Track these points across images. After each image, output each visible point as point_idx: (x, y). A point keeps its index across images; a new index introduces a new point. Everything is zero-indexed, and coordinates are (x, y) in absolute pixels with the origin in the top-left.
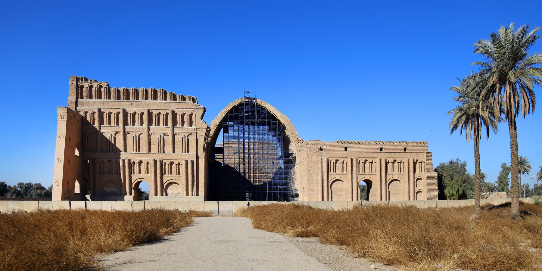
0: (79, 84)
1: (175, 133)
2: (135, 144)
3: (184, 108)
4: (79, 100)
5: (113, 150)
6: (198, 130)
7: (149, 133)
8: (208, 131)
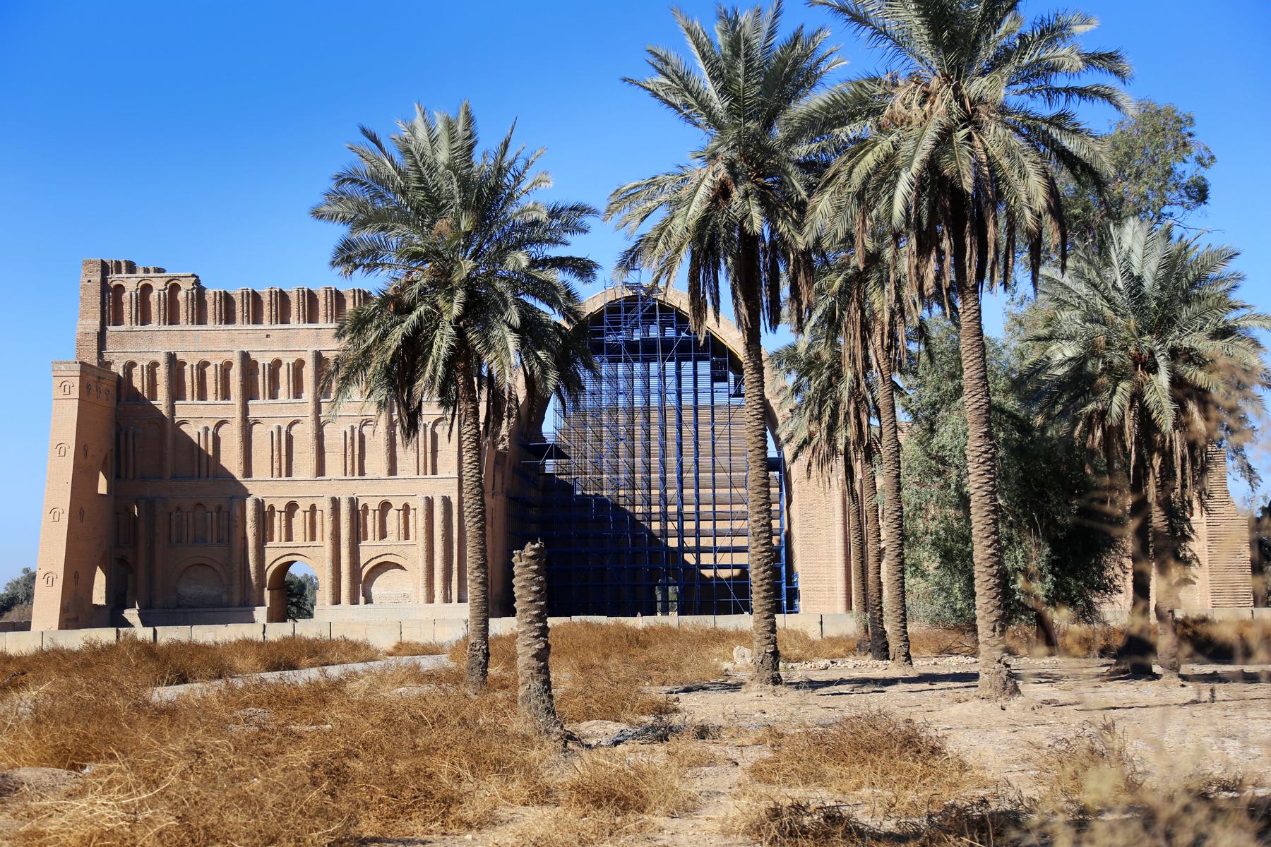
0: (109, 281)
2: (276, 453)
4: (110, 328)
5: (211, 474)
7: (317, 419)
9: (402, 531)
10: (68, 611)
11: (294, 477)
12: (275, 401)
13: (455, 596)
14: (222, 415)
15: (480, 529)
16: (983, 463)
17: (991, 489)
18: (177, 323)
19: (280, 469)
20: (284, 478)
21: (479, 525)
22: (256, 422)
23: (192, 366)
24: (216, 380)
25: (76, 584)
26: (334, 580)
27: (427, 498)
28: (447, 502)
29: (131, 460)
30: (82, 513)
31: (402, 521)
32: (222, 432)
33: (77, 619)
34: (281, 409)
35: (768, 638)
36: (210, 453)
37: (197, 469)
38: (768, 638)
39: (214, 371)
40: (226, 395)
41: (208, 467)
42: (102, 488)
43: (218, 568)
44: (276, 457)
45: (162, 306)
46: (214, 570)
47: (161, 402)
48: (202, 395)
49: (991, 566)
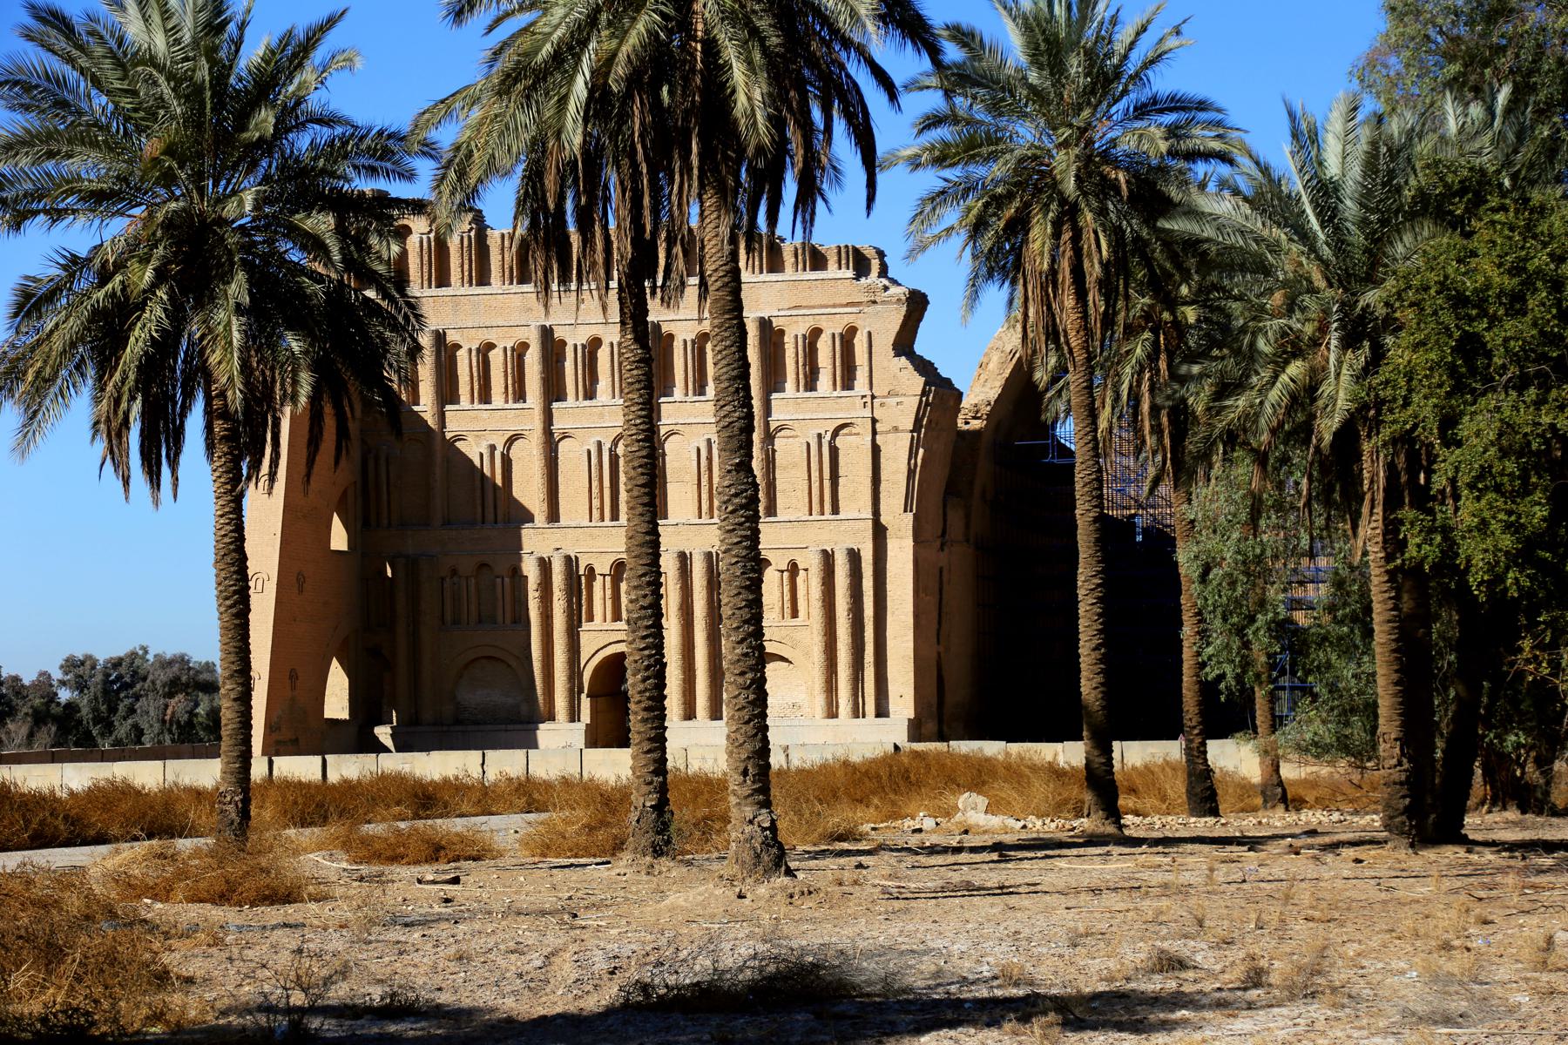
1: (773, 426)
2: (595, 484)
3: (813, 307)
5: (500, 517)
6: (882, 405)
8: (927, 404)
9: (787, 605)
10: (279, 729)
11: (563, 521)
12: (593, 402)
13: (870, 707)
14: (515, 427)
15: (236, 616)
16: (732, 512)
17: (744, 553)
18: (488, 284)
19: (602, 509)
20: (607, 522)
21: (234, 610)
22: (671, 434)
23: (470, 350)
24: (506, 371)
25: (293, 688)
26: (684, 681)
27: (824, 552)
28: (854, 557)
29: (385, 497)
30: (301, 580)
31: (786, 589)
32: (514, 453)
33: (295, 741)
34: (601, 416)
35: (650, 783)
36: (499, 481)
37: (479, 510)
38: (650, 783)
39: (501, 358)
40: (520, 395)
41: (495, 507)
42: (339, 539)
43: (514, 664)
44: (595, 491)
45: (426, 258)
46: (509, 666)
47: (426, 406)
48: (485, 397)
49: (742, 674)
